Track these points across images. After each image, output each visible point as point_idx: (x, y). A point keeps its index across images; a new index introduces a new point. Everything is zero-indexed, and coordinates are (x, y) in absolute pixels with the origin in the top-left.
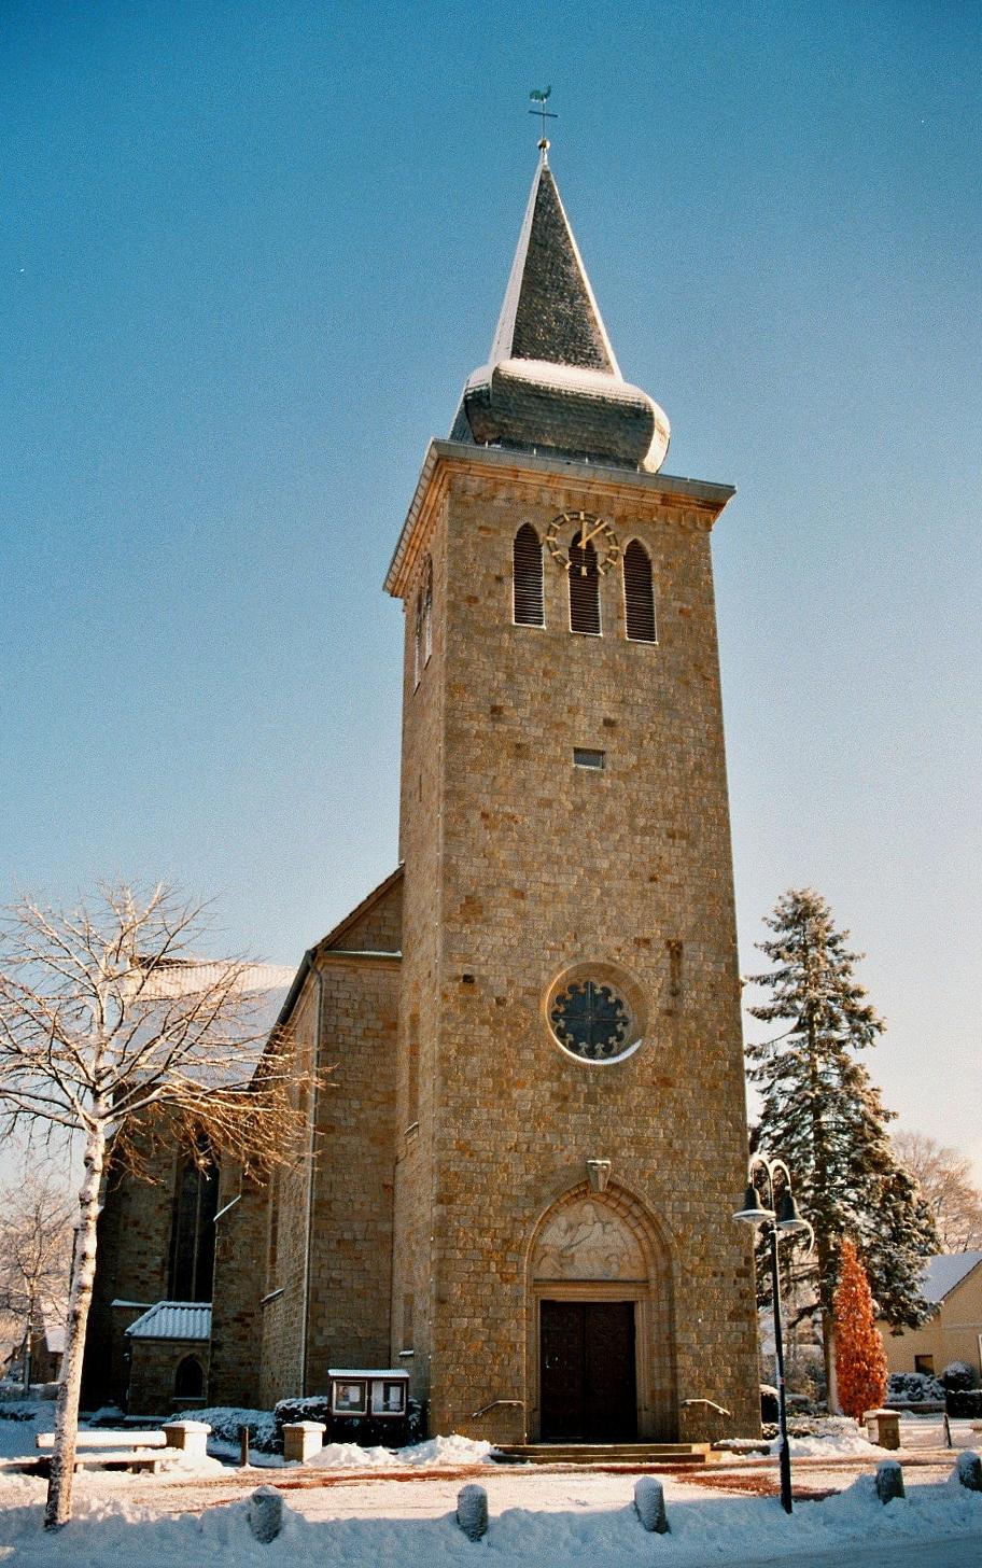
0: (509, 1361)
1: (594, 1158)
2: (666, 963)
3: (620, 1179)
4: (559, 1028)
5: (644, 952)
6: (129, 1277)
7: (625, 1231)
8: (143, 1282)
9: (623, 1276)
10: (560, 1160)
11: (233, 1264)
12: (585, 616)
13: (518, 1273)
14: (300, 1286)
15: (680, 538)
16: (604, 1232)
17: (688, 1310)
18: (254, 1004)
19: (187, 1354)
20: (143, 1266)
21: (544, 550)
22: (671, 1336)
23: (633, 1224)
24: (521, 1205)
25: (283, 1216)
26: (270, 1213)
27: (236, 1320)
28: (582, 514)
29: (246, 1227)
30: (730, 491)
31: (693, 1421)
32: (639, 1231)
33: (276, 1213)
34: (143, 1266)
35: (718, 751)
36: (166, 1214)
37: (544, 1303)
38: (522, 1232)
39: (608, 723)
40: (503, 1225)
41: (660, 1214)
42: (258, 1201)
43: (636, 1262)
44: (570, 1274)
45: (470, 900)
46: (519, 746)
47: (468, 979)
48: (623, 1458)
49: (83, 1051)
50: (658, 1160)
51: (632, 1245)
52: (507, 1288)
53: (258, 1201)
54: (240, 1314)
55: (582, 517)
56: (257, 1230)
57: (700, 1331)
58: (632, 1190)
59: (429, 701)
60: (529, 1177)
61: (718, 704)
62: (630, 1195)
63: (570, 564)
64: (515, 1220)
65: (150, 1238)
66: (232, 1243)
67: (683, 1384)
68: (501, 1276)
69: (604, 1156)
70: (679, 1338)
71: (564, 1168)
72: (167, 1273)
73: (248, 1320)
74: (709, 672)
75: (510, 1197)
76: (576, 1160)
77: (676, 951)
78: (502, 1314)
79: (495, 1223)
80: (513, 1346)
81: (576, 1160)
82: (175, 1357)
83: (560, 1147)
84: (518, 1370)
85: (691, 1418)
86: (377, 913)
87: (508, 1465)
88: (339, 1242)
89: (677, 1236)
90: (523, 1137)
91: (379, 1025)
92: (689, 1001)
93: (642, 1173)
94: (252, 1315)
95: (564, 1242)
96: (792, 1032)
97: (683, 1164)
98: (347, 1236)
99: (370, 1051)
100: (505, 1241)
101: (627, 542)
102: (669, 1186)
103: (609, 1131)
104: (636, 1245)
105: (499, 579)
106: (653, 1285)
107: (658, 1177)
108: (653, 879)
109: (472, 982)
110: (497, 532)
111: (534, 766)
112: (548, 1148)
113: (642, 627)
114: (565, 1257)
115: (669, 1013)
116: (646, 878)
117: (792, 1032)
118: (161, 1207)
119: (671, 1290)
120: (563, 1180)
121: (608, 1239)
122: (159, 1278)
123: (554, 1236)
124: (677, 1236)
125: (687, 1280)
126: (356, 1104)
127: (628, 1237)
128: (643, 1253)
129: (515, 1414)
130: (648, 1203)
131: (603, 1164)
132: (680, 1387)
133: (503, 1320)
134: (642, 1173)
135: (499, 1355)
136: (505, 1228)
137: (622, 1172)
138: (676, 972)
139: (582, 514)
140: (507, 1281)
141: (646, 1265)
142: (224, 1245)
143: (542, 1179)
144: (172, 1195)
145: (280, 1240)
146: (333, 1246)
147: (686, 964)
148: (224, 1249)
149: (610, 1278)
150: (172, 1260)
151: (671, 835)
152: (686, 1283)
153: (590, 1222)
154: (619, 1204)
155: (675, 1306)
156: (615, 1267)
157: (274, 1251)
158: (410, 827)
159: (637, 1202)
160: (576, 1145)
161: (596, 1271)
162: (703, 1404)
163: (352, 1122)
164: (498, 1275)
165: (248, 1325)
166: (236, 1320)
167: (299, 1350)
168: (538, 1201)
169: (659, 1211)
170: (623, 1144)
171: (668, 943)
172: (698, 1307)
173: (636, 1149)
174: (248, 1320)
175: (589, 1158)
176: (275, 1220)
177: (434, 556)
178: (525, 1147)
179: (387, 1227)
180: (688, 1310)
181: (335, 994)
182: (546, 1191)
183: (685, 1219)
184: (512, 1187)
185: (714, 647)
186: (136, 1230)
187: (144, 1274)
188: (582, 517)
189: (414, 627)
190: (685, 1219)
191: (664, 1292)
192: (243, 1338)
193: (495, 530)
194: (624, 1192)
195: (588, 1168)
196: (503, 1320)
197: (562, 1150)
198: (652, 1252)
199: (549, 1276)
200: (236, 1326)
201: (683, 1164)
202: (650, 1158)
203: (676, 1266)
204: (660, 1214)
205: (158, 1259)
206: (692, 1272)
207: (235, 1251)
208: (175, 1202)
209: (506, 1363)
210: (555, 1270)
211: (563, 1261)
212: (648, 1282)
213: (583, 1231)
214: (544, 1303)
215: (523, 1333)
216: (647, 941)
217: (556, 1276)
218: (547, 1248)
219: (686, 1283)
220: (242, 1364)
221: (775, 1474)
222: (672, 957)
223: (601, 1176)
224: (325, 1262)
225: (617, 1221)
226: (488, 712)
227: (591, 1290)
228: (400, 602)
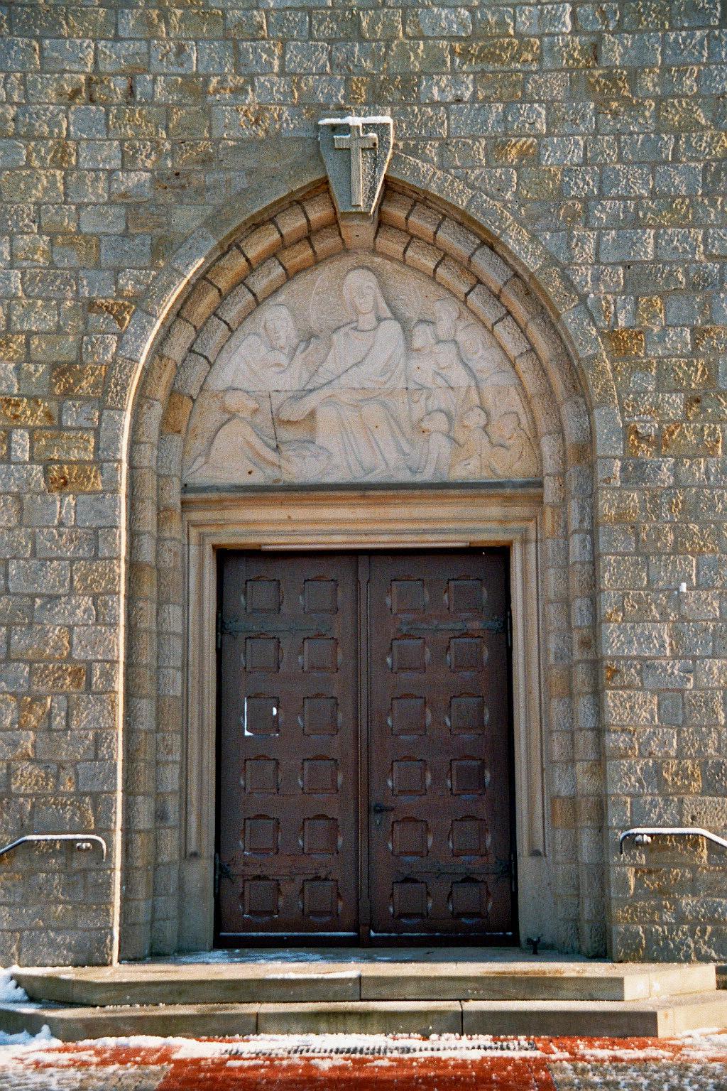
0: (68, 717)
1: (342, 111)
3: (426, 172)
7: (471, 338)
9: (460, 473)
10: (232, 123)
13: (98, 462)
16: (409, 349)
17: (644, 553)
22: (592, 641)
23: (490, 315)
24: (108, 259)
31: (662, 892)
32: (505, 333)
37: (225, 556)
38: (112, 340)
40: (50, 325)
41: (555, 271)
43: (505, 429)
44: (303, 467)
48: (364, 1016)
50: (550, 105)
51: (495, 380)
52: (65, 506)
57: (683, 618)
58: (462, 203)
60: (134, 179)
62: (466, 223)
64: (91, 305)
67: (626, 780)
68: (46, 472)
69: (376, 101)
70: (614, 642)
71: (245, 145)
75: (72, 240)
76: (289, 122)
78: (51, 578)
79: (25, 317)
80: (82, 674)
81: (289, 122)
83: (233, 81)
84: (97, 742)
85: (651, 883)
87: (586, 975)
89: (611, 335)
90: (114, 56)
93: (497, 147)
95: (290, 380)
97: (634, 108)
100: (59, 370)
102: (586, 184)
103: (389, 26)
104: (507, 380)
106: (551, 490)
107: (548, 159)
112: (194, 87)
114: (288, 426)
119: (590, 496)
120: (241, 182)
121: (424, 370)
123: (256, 362)
124: (611, 335)
125: (640, 466)
127: (483, 357)
128: (527, 399)
129: (85, 872)
130: (515, 240)
131: (367, 127)
132: (615, 789)
133: (53, 598)
134: (497, 147)
135: (38, 698)
136: (59, 330)
137: (432, 150)
140: (64, 484)
141: (534, 439)
143: (172, 182)
149: (426, 476)
152: (636, 473)
153: (367, 321)
154: (445, 257)
155: (602, 547)
156: (439, 447)
159: (490, 243)
160: (282, 73)
161: (384, 459)
162: (694, 840)
164: (37, 469)
168: (164, 248)
169: (552, 260)
170: (435, 64)
172: (677, 549)
173: (480, 76)
175: (323, 109)
178: (119, 86)
180: (644, 553)
182: (186, 217)
183: (638, 280)
184: (79, 207)
190: (638, 280)
191: (573, 506)
194: (446, 213)
195: (324, 143)
196: (53, 598)
197: (239, 91)
198: (549, 392)
199: (241, 478)
201: (634, 108)
202: (527, 99)
203: (607, 424)
204: (555, 271)
206: (659, 443)
209: (59, 722)
210: (258, 459)
211: (286, 434)
212: (540, 485)
213: (344, 348)
214: (225, 556)
217: (258, 479)
218: (232, 401)
219: (636, 473)
223: (361, 164)
225: (446, 313)
227: (361, 513)
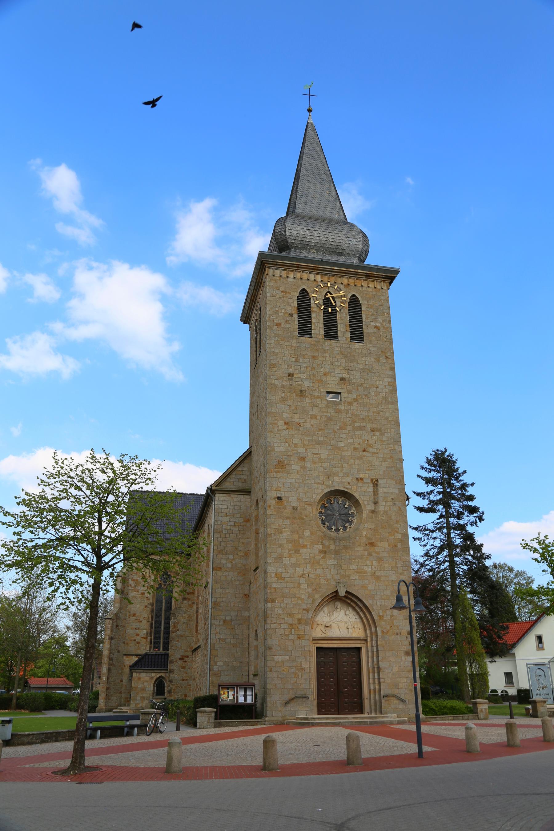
2: (371, 489)
4: (322, 520)
5: (360, 484)
6: (131, 640)
8: (138, 643)
11: (178, 633)
12: (331, 332)
14: (207, 642)
15: (374, 293)
18: (383, 360)
19: (158, 676)
20: (138, 635)
21: (312, 301)
25: (201, 610)
26: (195, 608)
27: (180, 659)
28: (329, 283)
29: (184, 615)
30: (397, 272)
33: (197, 608)
34: (138, 635)
35: (394, 390)
36: (149, 609)
39: (343, 379)
42: (190, 602)
45: (279, 462)
46: (301, 391)
47: (280, 498)
49: (100, 460)
53: (190, 602)
54: (182, 656)
55: (329, 285)
56: (190, 617)
59: (261, 372)
61: (393, 369)
63: (323, 307)
65: (141, 622)
66: (178, 623)
72: (149, 638)
73: (186, 659)
74: (389, 354)
77: (375, 483)
82: (152, 678)
86: (240, 469)
88: (224, 621)
91: (242, 520)
92: (382, 507)
94: (188, 657)
96: (438, 519)
98: (228, 618)
99: (238, 532)
101: (350, 295)
105: (291, 315)
108: (364, 451)
109: (281, 499)
110: (290, 293)
111: (308, 400)
113: (357, 334)
115: (373, 512)
116: (361, 450)
117: (438, 519)
118: (146, 607)
122: (145, 640)
126: (231, 557)
138: (376, 493)
139: (329, 283)
142: (174, 624)
144: (151, 601)
145: (199, 621)
146: (221, 623)
147: (380, 490)
148: (175, 627)
150: (151, 632)
151: (373, 430)
157: (197, 626)
158: (254, 429)
163: (229, 565)
165: (186, 662)
166: (180, 659)
167: (207, 673)
171: (372, 480)
174: (186, 659)
176: (197, 612)
177: (261, 305)
179: (246, 614)
181: (221, 506)
185: (391, 343)
186: (134, 618)
187: (138, 639)
188: (329, 285)
189: (254, 338)
192: (184, 668)
193: (289, 293)
200: (180, 663)
205: (145, 632)
207: (179, 627)
208: (152, 604)
214: (317, 648)
215: (310, 663)
216: (362, 479)
220: (183, 680)
221: (414, 728)
222: (373, 486)
224: (218, 631)
226: (287, 376)
228: (247, 326)
